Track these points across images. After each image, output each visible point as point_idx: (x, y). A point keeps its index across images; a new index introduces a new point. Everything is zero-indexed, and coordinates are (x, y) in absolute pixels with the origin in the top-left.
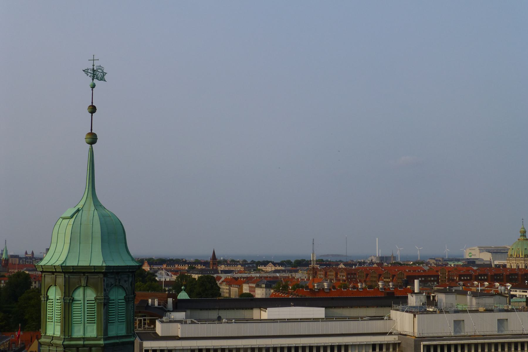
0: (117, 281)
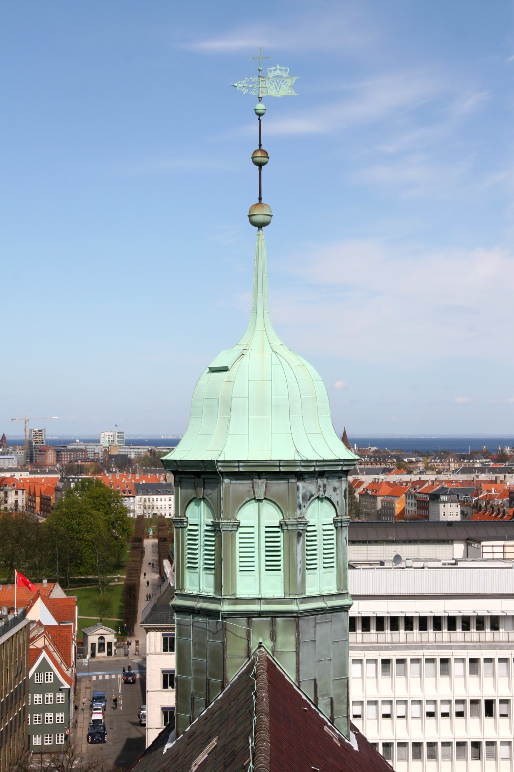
0: (322, 489)
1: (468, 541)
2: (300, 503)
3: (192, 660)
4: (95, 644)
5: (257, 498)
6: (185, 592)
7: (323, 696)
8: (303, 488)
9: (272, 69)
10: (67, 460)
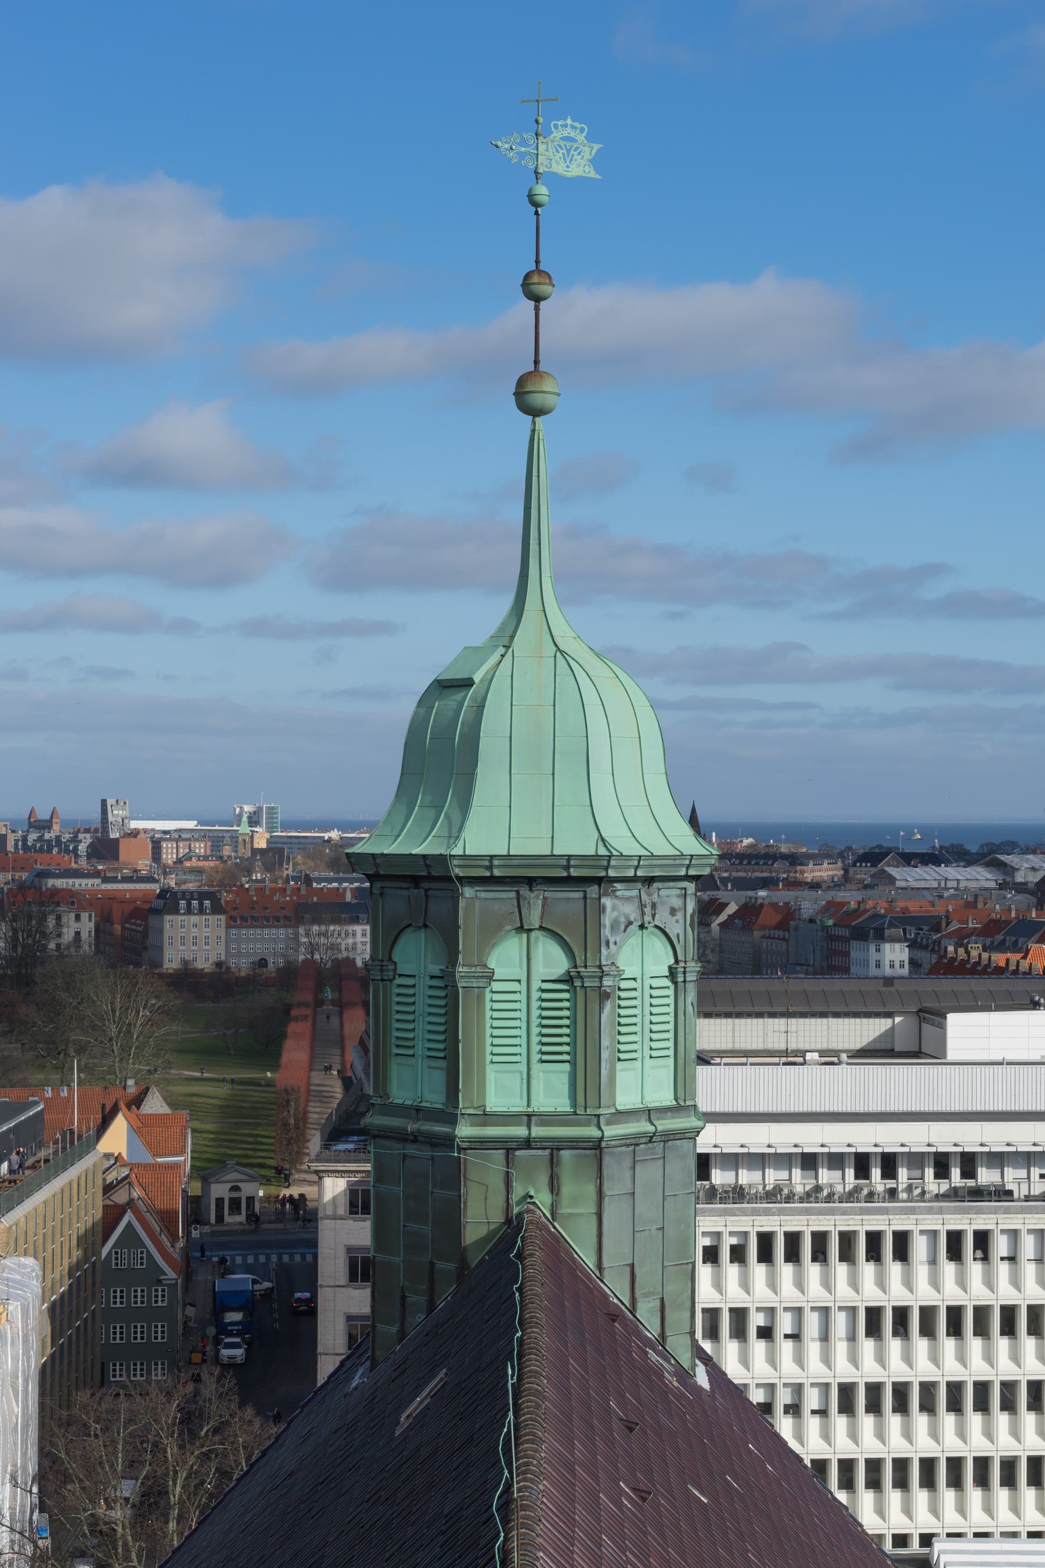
0: (648, 910)
1: (921, 1014)
2: (607, 936)
3: (402, 1227)
4: (223, 1199)
5: (525, 928)
6: (390, 1101)
7: (646, 1295)
8: (614, 908)
9: (560, 123)
10: (172, 858)
